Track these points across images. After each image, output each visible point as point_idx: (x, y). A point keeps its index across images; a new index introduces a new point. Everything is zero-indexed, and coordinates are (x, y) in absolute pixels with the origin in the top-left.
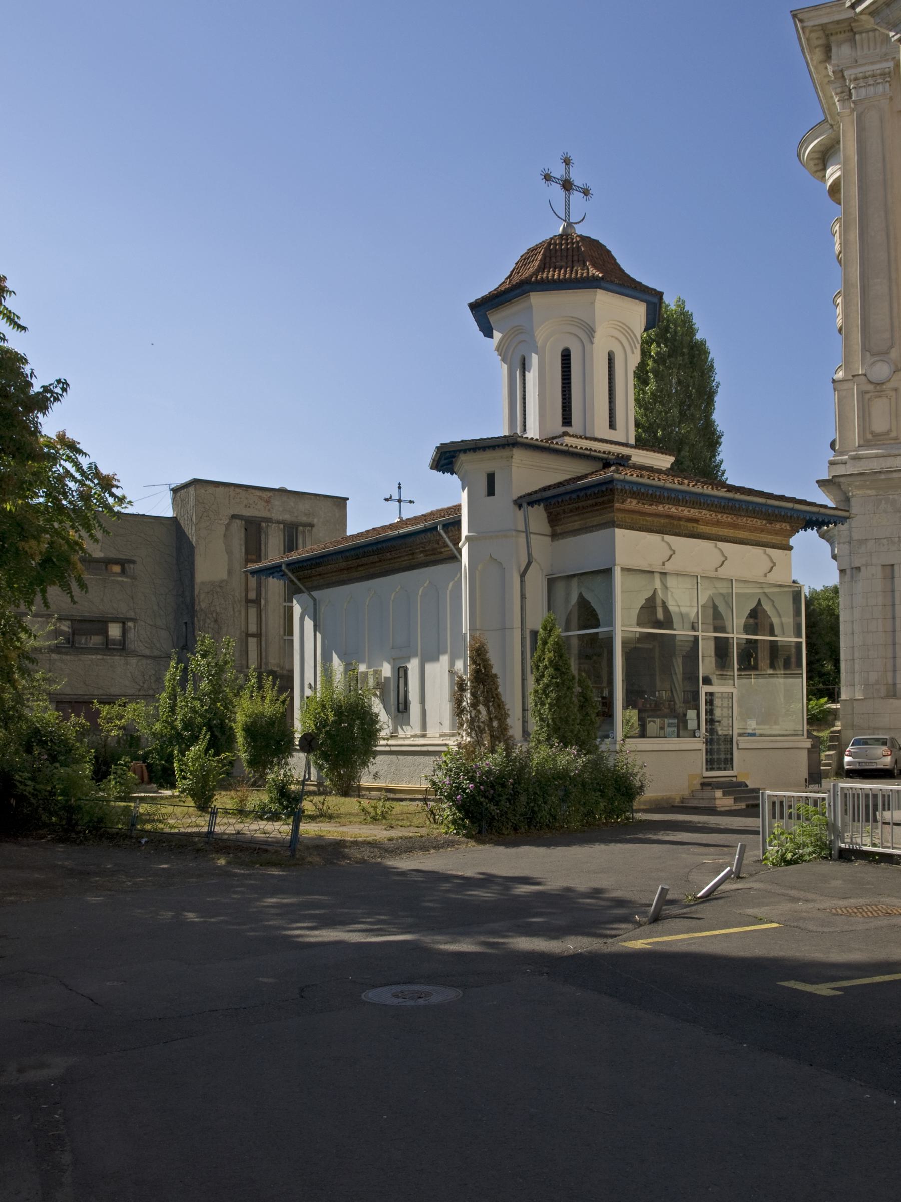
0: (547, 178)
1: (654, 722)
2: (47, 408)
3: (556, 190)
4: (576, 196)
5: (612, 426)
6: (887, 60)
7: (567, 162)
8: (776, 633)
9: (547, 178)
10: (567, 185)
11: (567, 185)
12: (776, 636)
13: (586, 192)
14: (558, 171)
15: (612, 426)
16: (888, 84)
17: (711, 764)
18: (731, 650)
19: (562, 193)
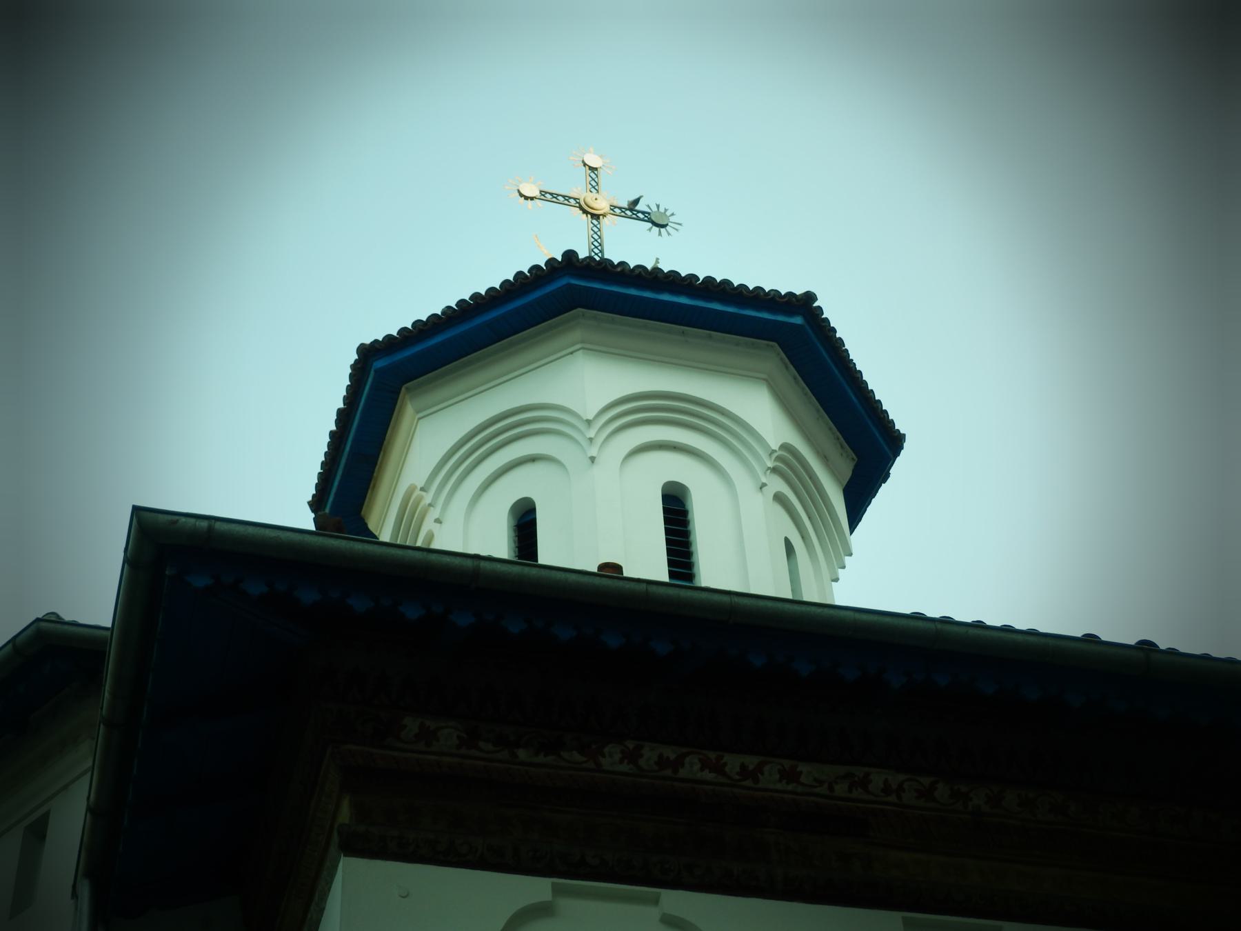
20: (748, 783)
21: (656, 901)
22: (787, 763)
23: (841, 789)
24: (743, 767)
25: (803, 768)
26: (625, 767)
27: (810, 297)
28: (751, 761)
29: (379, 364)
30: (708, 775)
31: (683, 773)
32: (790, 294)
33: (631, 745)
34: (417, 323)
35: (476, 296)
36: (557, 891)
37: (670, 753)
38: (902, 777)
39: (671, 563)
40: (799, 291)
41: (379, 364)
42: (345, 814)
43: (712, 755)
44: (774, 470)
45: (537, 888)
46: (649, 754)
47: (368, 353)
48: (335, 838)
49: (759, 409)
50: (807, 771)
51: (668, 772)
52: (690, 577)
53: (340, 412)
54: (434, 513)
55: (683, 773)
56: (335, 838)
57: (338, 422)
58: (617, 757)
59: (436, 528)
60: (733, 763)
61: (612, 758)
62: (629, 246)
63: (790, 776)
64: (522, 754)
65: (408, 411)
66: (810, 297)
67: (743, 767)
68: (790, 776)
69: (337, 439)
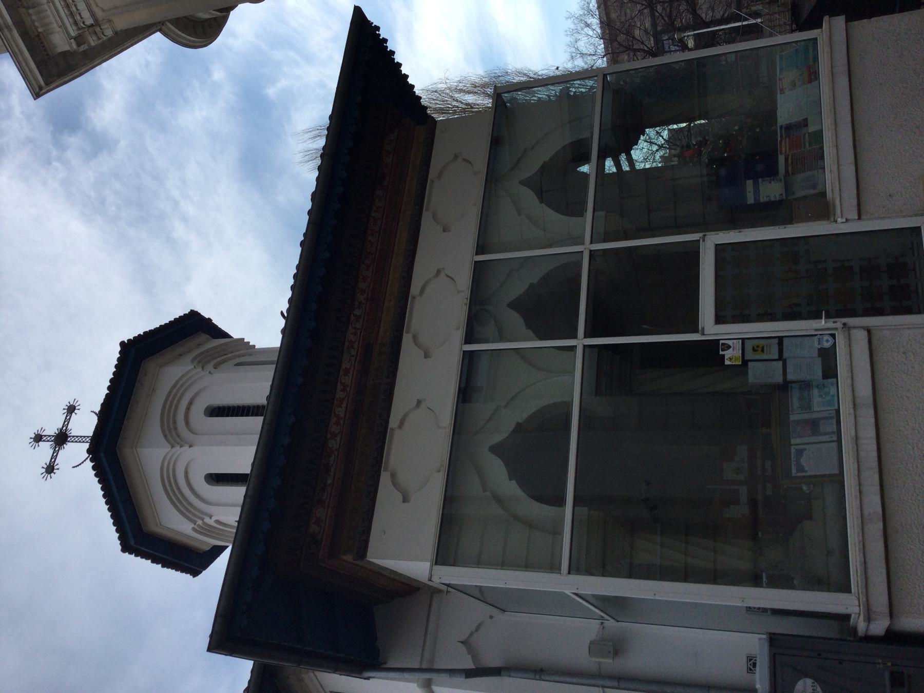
0: (50, 469)
1: (800, 453)
7: (38, 438)
9: (50, 469)
10: (61, 438)
11: (61, 438)
20: (348, 389)
21: (392, 430)
22: (341, 373)
23: (353, 352)
24: (342, 391)
25: (344, 366)
26: (338, 439)
27: (122, 344)
28: (339, 387)
29: (132, 543)
30: (344, 405)
31: (342, 415)
32: (120, 352)
33: (329, 436)
34: (114, 524)
35: (104, 496)
36: (386, 470)
37: (334, 420)
38: (350, 327)
39: (257, 415)
40: (119, 349)
41: (132, 543)
42: (349, 558)
43: (336, 402)
44: (203, 367)
45: (385, 478)
46: (334, 428)
47: (127, 547)
48: (358, 562)
49: (171, 373)
50: (345, 365)
51: (341, 421)
52: (263, 407)
53: (153, 562)
54: (207, 520)
55: (342, 415)
56: (358, 562)
57: (157, 563)
58: (333, 441)
59: (214, 518)
60: (340, 394)
61: (334, 444)
62: (85, 424)
63: (347, 371)
64: (329, 482)
65: (153, 528)
66: (122, 344)
67: (342, 391)
68: (347, 371)
69: (166, 564)
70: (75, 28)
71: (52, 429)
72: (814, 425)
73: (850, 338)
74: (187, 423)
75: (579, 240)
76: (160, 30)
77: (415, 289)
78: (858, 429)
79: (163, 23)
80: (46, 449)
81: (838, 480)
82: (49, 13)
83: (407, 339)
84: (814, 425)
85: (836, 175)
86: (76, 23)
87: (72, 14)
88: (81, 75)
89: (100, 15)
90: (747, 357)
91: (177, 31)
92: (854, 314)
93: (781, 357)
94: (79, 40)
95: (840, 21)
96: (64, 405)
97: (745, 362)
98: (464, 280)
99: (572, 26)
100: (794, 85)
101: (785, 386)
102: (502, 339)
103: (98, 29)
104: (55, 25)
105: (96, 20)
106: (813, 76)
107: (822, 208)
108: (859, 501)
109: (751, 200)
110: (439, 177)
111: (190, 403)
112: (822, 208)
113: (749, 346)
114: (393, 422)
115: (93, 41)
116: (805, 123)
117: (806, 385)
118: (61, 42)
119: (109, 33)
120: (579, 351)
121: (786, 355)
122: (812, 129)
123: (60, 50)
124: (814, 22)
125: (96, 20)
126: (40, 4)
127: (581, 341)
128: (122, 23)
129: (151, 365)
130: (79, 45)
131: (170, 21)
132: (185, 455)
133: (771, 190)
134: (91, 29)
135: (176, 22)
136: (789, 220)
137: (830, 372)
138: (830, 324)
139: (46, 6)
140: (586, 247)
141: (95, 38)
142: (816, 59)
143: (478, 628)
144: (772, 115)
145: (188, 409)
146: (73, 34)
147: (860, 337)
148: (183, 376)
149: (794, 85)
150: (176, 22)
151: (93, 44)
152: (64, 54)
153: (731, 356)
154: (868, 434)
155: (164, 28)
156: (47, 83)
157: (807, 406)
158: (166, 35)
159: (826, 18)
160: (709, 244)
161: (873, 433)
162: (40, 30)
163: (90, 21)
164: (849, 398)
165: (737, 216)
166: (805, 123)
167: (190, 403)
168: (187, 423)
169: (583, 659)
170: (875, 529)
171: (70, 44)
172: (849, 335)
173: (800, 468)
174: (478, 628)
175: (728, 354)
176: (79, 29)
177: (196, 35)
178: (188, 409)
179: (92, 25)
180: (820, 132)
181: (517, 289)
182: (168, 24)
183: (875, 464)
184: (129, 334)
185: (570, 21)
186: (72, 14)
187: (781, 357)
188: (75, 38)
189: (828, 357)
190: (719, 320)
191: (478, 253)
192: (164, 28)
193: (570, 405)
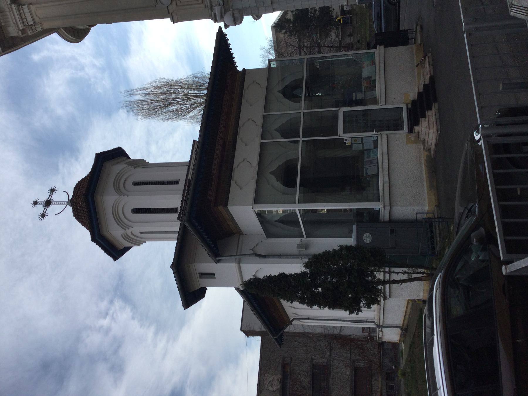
0: (43, 216)
1: (367, 169)
2: (322, 9)
3: (52, 208)
4: (55, 197)
5: (177, 182)
6: (12, 8)
7: (36, 203)
8: (301, 77)
9: (43, 216)
10: (48, 203)
11: (48, 203)
12: (303, 78)
13: (53, 191)
14: (40, 209)
15: (177, 182)
16: (23, 7)
17: (398, 126)
18: (319, 331)
19: (52, 206)
27: (96, 154)
45: (233, 183)
60: (215, 156)
66: (96, 154)
70: (22, 25)
71: (43, 198)
72: (371, 162)
73: (382, 137)
74: (124, 187)
75: (300, 109)
76: (57, 32)
77: (240, 124)
78: (382, 161)
79: (59, 29)
80: (40, 209)
81: (377, 175)
82: (9, 16)
83: (238, 141)
84: (371, 162)
85: (380, 92)
86: (23, 23)
87: (22, 18)
88: (18, 49)
89: (37, 20)
90: (353, 142)
91: (67, 34)
92: (383, 131)
93: (362, 143)
94: (23, 31)
95: (382, 47)
96: (49, 189)
97: (352, 144)
98: (260, 122)
99: (264, 53)
100: (368, 66)
101: (362, 152)
102: (273, 138)
103: (33, 27)
104: (12, 22)
105: (35, 22)
106: (373, 63)
107: (375, 101)
108: (383, 179)
109: (354, 99)
110: (248, 88)
111: (125, 180)
112: (375, 101)
113: (353, 139)
114: (235, 165)
115: (30, 33)
116: (371, 77)
117: (369, 150)
118: (13, 31)
119: (39, 29)
120: (301, 142)
121: (363, 142)
122: (373, 79)
123: (12, 35)
124: (375, 47)
125: (35, 22)
126: (5, 12)
127: (301, 139)
128: (46, 26)
129: (107, 164)
130: (23, 34)
131: (63, 28)
132: (124, 200)
133: (359, 96)
134: (30, 27)
135: (65, 29)
136: (365, 105)
137: (376, 147)
138: (376, 133)
139: (8, 13)
140: (302, 111)
141: (31, 31)
142: (375, 58)
143: (257, 245)
144: (361, 75)
145: (124, 183)
146: (21, 28)
147: (385, 137)
148: (122, 169)
149: (368, 66)
150: (65, 29)
151: (30, 34)
152: (12, 37)
153: (348, 142)
154: (386, 161)
155: (59, 31)
156: (3, 51)
157: (369, 156)
158: (60, 35)
159: (378, 46)
160: (341, 111)
161: (387, 172)
162: (3, 24)
163: (32, 23)
164: (381, 152)
165: (351, 103)
166: (371, 77)
167: (125, 180)
168: (124, 187)
169: (295, 251)
170: (387, 185)
171: (18, 33)
172: (397, 327)
173: (367, 174)
174: (257, 245)
175: (347, 142)
176: (24, 26)
177: (74, 36)
178: (124, 183)
179: (31, 25)
180: (375, 80)
181: (278, 124)
182: (62, 29)
183: (387, 169)
184: (100, 151)
185: (262, 51)
186: (22, 18)
187: (362, 143)
188: (21, 30)
189: (375, 142)
190: (344, 132)
191: (264, 112)
192: (59, 31)
193: (297, 160)
